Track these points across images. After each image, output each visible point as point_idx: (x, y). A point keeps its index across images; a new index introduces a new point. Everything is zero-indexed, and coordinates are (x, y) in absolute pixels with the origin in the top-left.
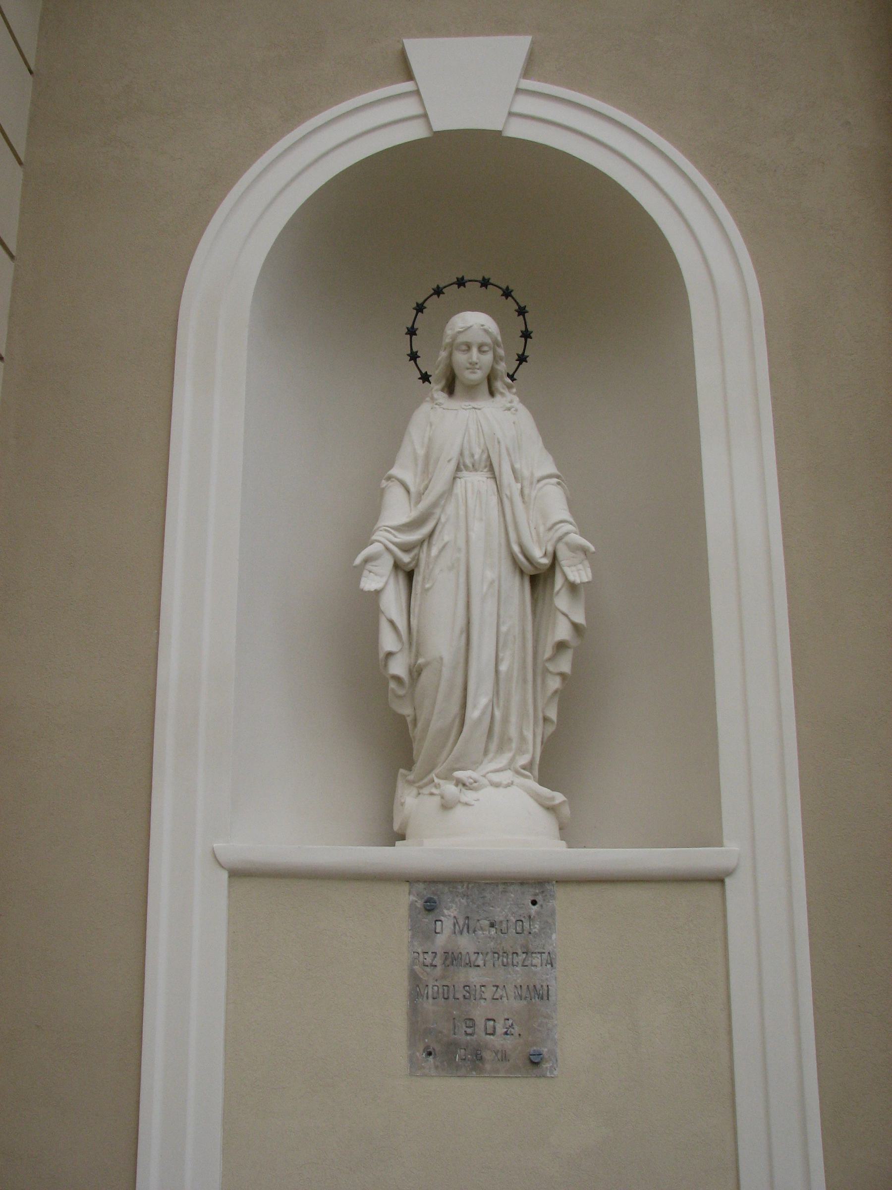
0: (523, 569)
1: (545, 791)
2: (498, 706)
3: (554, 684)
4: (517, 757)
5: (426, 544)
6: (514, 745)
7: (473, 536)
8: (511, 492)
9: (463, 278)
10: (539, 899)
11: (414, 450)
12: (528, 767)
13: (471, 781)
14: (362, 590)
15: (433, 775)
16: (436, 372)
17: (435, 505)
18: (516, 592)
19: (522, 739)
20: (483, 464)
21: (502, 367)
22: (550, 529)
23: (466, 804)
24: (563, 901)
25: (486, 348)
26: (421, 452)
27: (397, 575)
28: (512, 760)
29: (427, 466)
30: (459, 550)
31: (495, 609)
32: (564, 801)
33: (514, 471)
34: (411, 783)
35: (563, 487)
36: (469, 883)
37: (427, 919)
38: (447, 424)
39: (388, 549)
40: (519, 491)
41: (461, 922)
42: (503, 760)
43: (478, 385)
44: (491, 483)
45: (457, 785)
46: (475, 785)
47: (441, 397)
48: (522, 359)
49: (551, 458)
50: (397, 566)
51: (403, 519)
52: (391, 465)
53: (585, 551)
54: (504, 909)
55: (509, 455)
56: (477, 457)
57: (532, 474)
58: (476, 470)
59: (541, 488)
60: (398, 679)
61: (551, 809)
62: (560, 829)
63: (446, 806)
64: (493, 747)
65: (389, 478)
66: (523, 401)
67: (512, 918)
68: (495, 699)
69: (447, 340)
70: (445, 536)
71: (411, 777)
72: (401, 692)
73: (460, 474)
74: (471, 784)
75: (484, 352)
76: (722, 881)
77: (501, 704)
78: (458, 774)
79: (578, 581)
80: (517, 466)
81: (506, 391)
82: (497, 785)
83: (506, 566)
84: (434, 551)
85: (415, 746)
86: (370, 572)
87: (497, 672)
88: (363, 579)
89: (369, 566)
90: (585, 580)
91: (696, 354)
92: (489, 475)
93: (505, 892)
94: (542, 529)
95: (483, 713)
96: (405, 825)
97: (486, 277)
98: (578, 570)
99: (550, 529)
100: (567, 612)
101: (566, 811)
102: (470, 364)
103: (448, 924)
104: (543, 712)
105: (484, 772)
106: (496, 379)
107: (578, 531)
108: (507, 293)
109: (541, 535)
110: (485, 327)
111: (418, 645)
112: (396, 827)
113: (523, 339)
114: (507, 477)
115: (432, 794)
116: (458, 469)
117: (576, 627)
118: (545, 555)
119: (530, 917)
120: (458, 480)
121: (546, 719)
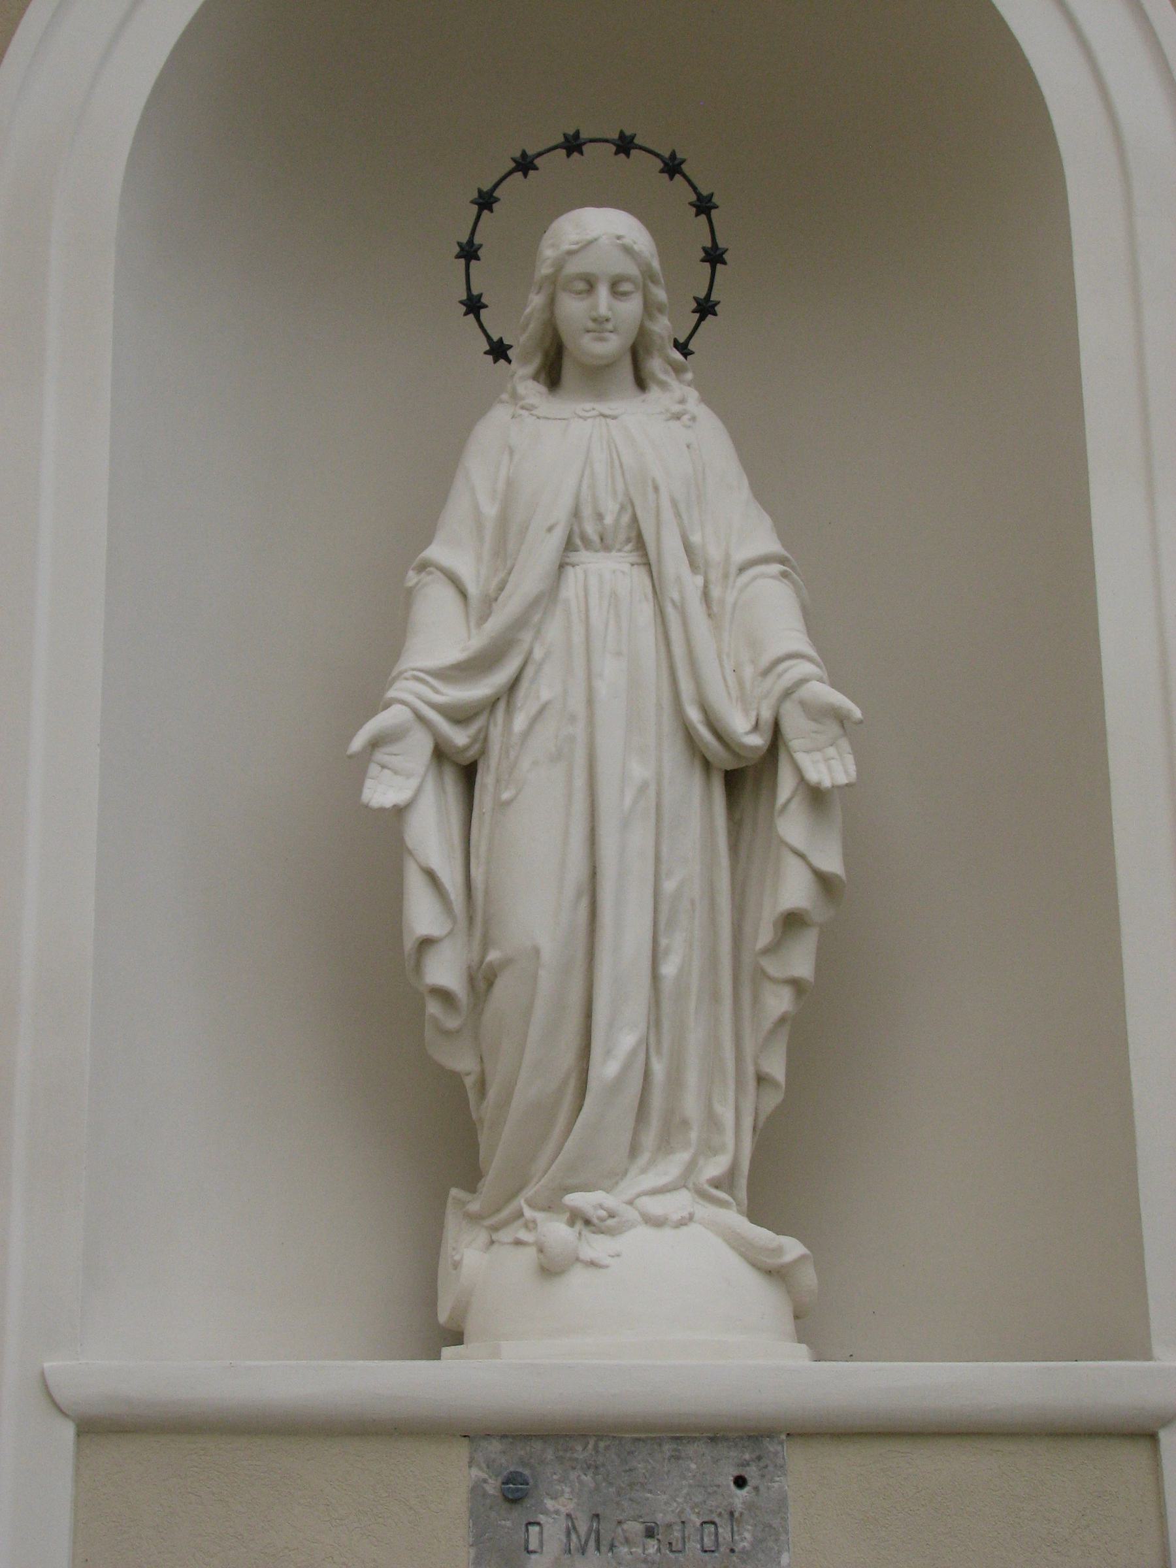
0: (710, 759)
1: (762, 1235)
2: (659, 1052)
3: (779, 1002)
4: (701, 1162)
5: (502, 705)
6: (693, 1135)
7: (602, 689)
8: (681, 592)
9: (577, 135)
10: (751, 1473)
11: (476, 508)
12: (726, 1182)
13: (603, 1213)
14: (367, 806)
15: (521, 1201)
16: (522, 339)
17: (520, 623)
18: (696, 807)
19: (712, 1121)
20: (622, 536)
21: (662, 327)
22: (766, 672)
23: (593, 1264)
24: (801, 1474)
25: (626, 287)
26: (490, 510)
27: (440, 774)
28: (691, 1168)
29: (503, 542)
30: (573, 719)
31: (651, 843)
32: (803, 1258)
33: (688, 548)
34: (475, 1219)
35: (793, 582)
36: (600, 1438)
37: (508, 1521)
38: (547, 450)
39: (420, 718)
40: (699, 592)
41: (583, 1528)
42: (672, 1168)
43: (608, 366)
44: (639, 576)
45: (571, 1223)
46: (610, 1222)
47: (533, 392)
48: (705, 308)
49: (767, 521)
50: (441, 754)
51: (452, 653)
52: (428, 541)
53: (840, 718)
54: (674, 1496)
55: (678, 515)
56: (609, 520)
57: (727, 557)
58: (607, 548)
59: (747, 585)
60: (444, 996)
61: (776, 1274)
62: (796, 1317)
63: (550, 1269)
64: (649, 1139)
65: (423, 567)
66: (705, 399)
67: (694, 1518)
68: (652, 1040)
69: (545, 270)
70: (542, 689)
71: (474, 1207)
72: (452, 1023)
73: (574, 557)
74: (602, 1220)
75: (625, 294)
76: (1152, 1437)
77: (666, 1044)
78: (575, 1199)
79: (827, 783)
80: (696, 538)
81: (671, 379)
82: (657, 1222)
83: (673, 753)
84: (520, 722)
85: (483, 1138)
86: (383, 767)
87: (655, 977)
88: (369, 783)
89: (380, 755)
90: (842, 779)
91: (1079, 284)
92: (634, 557)
93: (678, 1458)
94: (748, 672)
95: (626, 1067)
96: (461, 1310)
97: (628, 133)
98: (827, 760)
99: (766, 672)
100: (802, 850)
101: (809, 1278)
102: (595, 320)
103: (553, 1531)
104: (756, 1064)
105: (628, 1195)
106: (649, 352)
107: (825, 677)
108: (672, 167)
109: (748, 685)
110: (627, 241)
111: (487, 922)
112: (443, 1317)
113: (707, 265)
114: (673, 561)
115: (518, 1243)
116: (569, 546)
117: (824, 881)
118: (756, 727)
119: (732, 1514)
120: (570, 571)
121: (761, 1079)
